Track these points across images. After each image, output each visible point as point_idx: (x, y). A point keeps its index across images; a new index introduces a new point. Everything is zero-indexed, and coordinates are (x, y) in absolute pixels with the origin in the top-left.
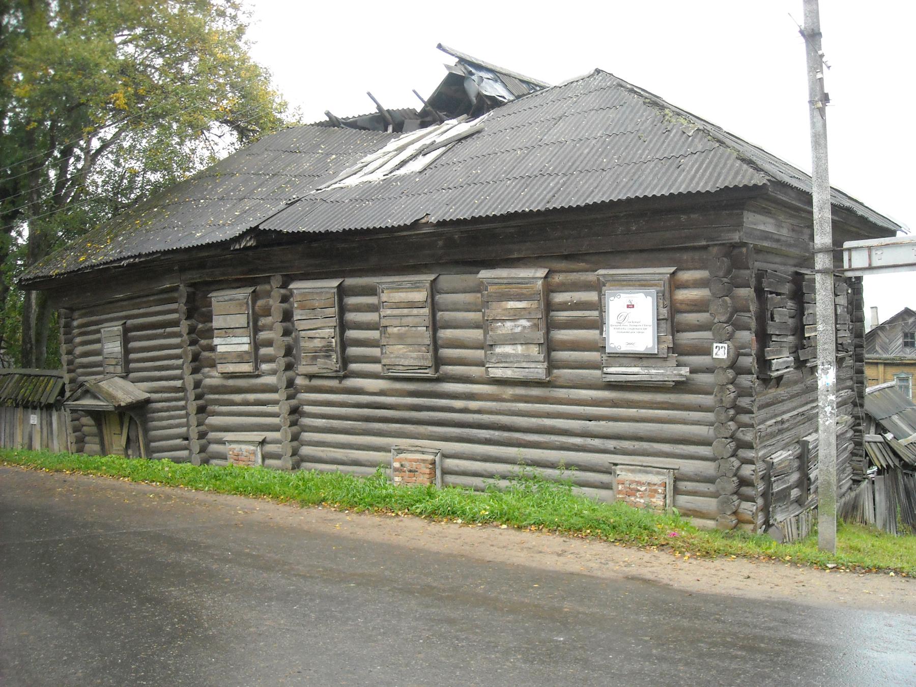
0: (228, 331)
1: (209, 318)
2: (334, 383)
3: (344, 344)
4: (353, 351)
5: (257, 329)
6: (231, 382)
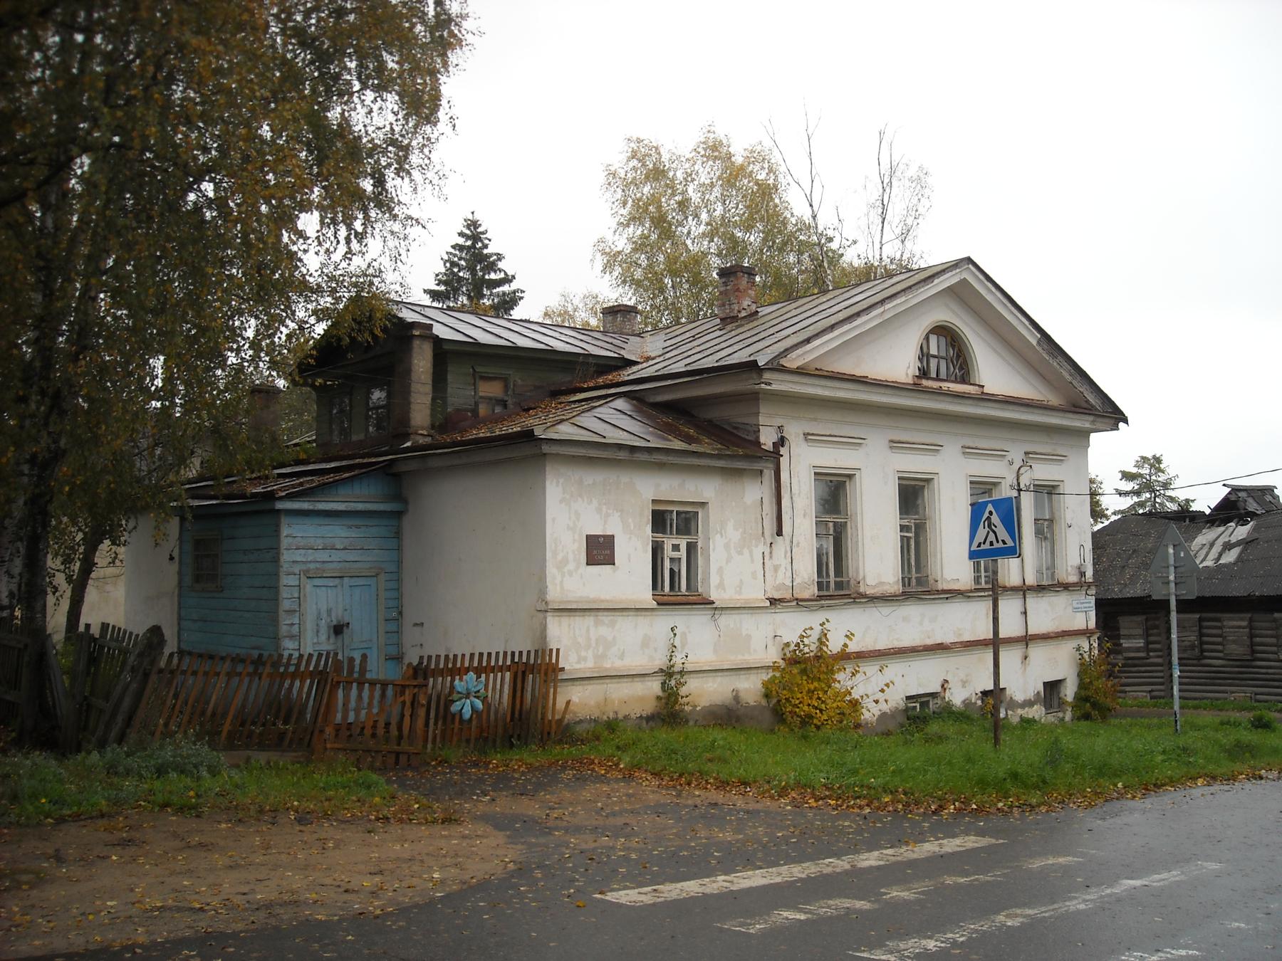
0: (1129, 637)
1: (1118, 629)
2: (1195, 662)
3: (1202, 643)
4: (1205, 647)
5: (1148, 635)
6: (1130, 662)
